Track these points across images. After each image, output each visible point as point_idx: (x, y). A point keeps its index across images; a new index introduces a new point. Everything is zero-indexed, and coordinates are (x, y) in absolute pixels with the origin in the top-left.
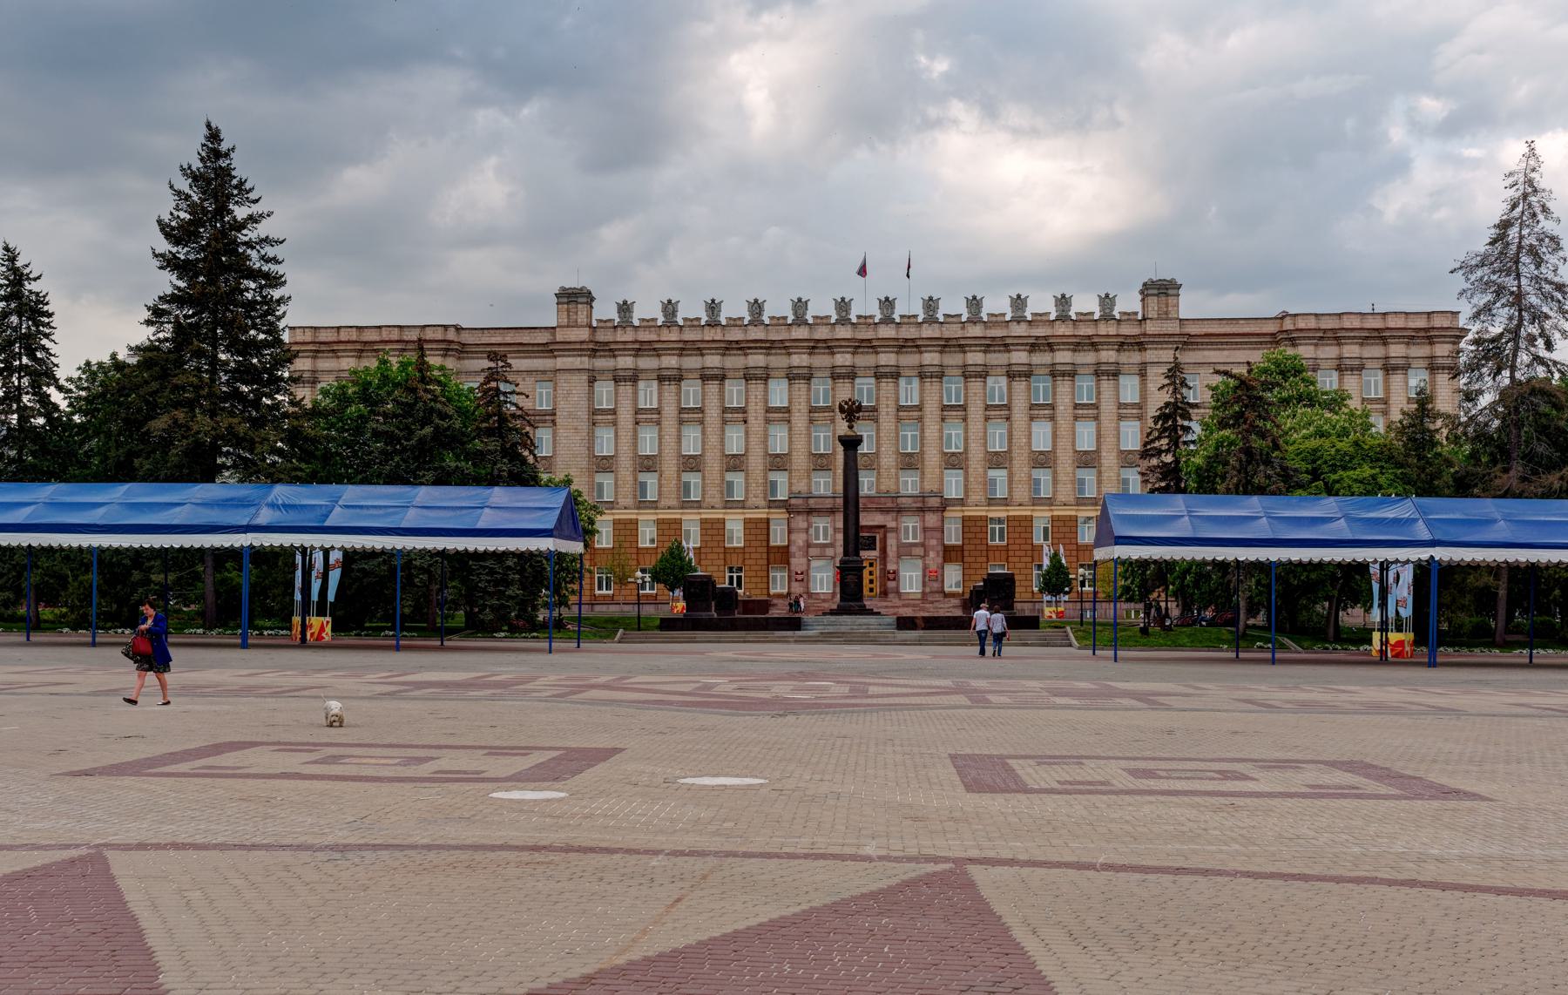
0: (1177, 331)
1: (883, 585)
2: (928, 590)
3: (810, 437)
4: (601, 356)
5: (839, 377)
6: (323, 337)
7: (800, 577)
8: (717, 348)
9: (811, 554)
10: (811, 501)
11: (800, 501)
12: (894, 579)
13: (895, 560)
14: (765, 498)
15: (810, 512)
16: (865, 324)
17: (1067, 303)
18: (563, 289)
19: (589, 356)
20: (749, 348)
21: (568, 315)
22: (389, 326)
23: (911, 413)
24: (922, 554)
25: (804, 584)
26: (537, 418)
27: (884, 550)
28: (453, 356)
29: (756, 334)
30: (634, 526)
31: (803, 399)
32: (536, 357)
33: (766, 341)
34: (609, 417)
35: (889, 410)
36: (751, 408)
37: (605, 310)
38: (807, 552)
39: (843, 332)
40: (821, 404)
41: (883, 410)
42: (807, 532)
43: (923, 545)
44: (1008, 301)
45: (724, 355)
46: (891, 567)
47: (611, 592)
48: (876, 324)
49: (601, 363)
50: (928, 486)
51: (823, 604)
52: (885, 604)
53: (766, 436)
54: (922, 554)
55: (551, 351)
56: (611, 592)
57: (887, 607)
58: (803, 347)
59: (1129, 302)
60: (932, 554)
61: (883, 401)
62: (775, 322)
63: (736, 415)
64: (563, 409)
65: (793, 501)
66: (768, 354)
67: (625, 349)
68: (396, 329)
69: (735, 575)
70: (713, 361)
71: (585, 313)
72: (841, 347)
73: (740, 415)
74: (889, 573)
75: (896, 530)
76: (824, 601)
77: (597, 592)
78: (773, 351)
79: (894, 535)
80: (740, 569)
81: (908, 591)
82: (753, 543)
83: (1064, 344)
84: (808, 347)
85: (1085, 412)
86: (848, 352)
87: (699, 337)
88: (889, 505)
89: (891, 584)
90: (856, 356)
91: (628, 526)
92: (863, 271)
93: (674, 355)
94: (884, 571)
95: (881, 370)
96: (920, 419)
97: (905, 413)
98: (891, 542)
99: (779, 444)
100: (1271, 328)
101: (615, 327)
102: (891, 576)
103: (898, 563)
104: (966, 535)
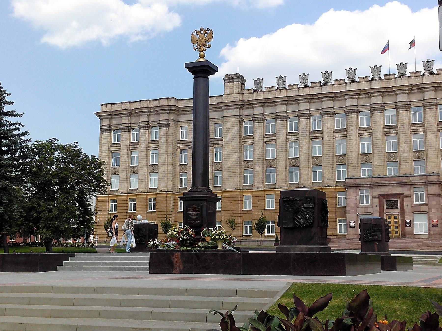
1: (403, 230)
2: (432, 233)
3: (359, 145)
4: (246, 108)
5: (374, 110)
6: (115, 108)
8: (305, 99)
10: (411, 178)
11: (352, 181)
12: (410, 226)
15: (357, 187)
16: (389, 79)
18: (227, 75)
19: (240, 108)
20: (323, 97)
21: (230, 88)
22: (144, 100)
23: (419, 128)
24: (427, 211)
26: (215, 142)
27: (403, 209)
28: (174, 113)
29: (328, 90)
30: (263, 198)
31: (354, 124)
32: (214, 111)
33: (383, 88)
34: (251, 140)
35: (405, 126)
36: (325, 130)
37: (250, 84)
38: (356, 210)
39: (377, 85)
41: (401, 127)
42: (356, 199)
43: (427, 205)
44: (276, 80)
45: (310, 102)
46: (407, 219)
47: (251, 234)
48: (395, 78)
49: (246, 112)
50: (431, 171)
53: (264, 150)
54: (427, 211)
55: (221, 107)
56: (251, 234)
58: (353, 95)
60: (433, 210)
61: (401, 122)
62: (337, 82)
63: (317, 135)
64: (226, 136)
65: (348, 181)
66: (334, 101)
67: (257, 104)
68: (129, 103)
70: (304, 106)
71: (238, 86)
72: (375, 92)
73: (320, 135)
75: (410, 196)
78: (337, 99)
79: (409, 199)
84: (356, 95)
86: (379, 96)
87: (273, 96)
89: (407, 229)
90: (385, 98)
91: (260, 198)
93: (283, 104)
94: (404, 221)
95: (426, 101)
96: (424, 131)
98: (407, 202)
99: (271, 153)
101: (346, 83)
102: (408, 224)
104: (224, 206)
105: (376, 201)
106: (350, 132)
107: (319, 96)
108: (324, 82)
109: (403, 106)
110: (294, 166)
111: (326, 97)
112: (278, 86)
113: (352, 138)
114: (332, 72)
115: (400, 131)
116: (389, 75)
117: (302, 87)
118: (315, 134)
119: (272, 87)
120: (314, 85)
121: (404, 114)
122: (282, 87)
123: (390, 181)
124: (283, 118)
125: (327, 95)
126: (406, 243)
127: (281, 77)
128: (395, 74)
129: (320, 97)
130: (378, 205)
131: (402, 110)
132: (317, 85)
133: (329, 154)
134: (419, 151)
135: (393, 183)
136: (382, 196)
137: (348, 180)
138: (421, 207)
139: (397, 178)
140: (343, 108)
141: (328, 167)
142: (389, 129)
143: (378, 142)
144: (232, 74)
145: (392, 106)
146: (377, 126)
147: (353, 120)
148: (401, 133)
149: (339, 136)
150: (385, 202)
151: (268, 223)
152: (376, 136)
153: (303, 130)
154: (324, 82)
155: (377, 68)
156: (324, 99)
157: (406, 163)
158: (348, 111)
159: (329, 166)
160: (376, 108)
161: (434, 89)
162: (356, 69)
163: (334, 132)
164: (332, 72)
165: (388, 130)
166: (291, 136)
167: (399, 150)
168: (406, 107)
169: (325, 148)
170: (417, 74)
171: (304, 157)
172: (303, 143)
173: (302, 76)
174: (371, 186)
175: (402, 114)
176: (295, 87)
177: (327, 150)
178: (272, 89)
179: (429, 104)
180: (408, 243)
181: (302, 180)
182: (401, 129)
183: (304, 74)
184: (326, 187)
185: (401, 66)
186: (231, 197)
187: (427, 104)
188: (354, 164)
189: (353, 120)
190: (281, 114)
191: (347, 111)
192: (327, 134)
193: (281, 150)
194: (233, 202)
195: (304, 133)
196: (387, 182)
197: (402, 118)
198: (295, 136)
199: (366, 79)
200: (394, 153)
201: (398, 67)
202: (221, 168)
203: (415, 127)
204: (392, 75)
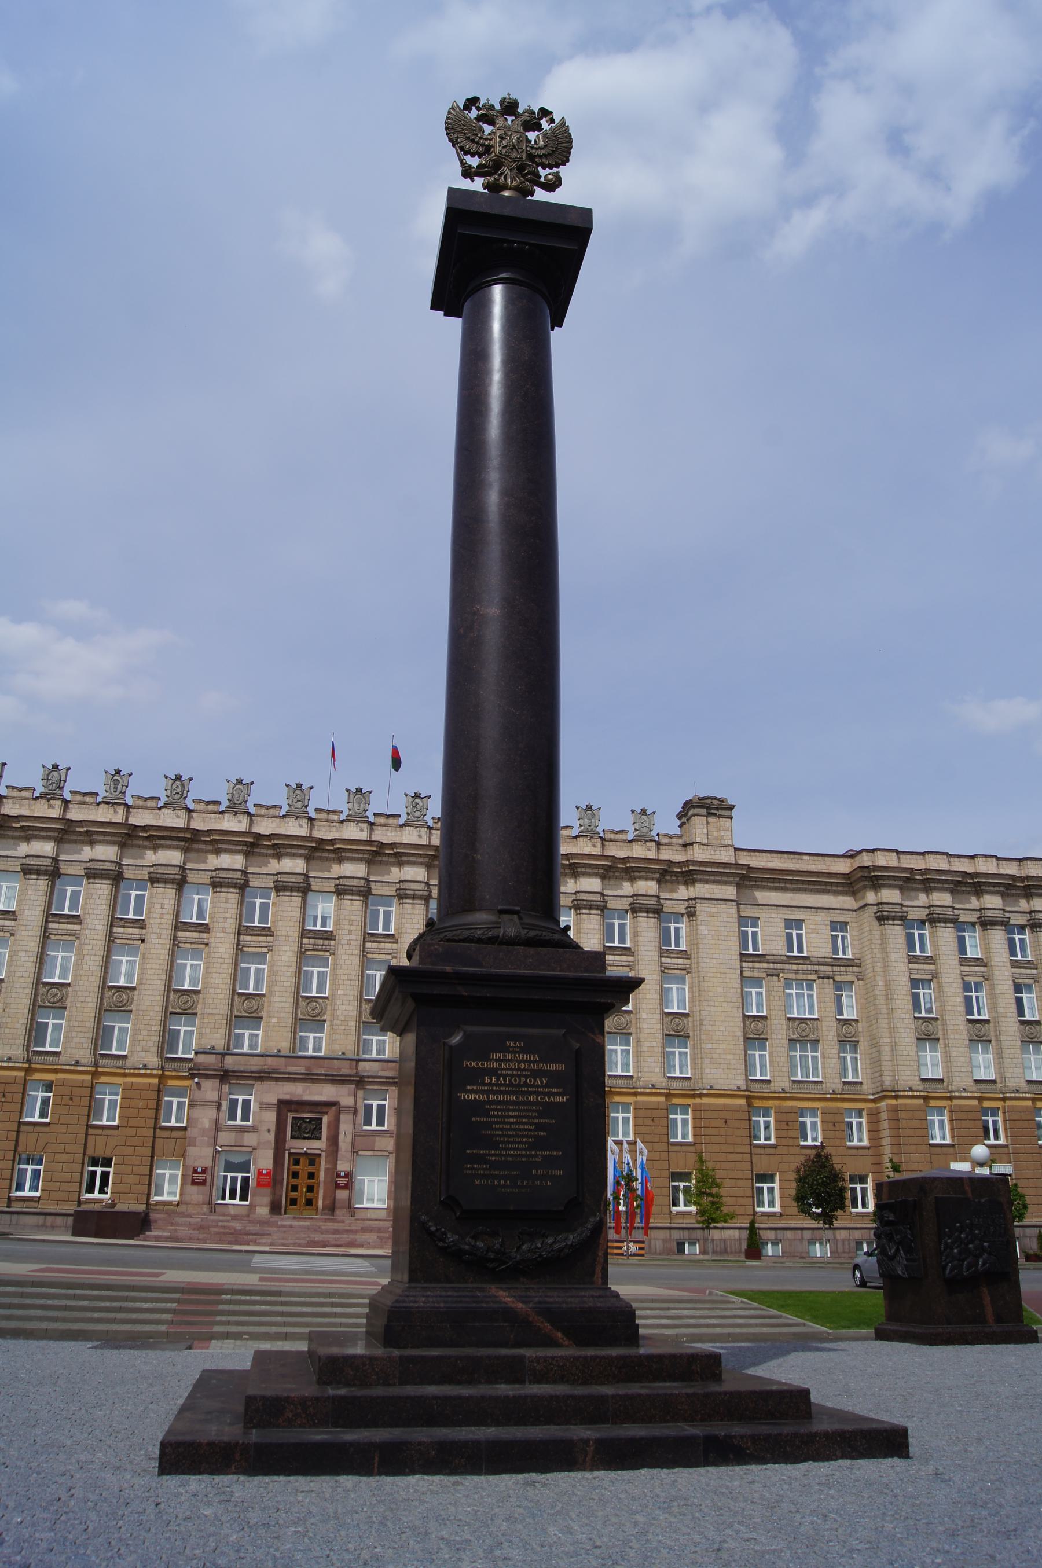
0: (597, 851)
7: (200, 1178)
9: (220, 1141)
13: (349, 1156)
14: (160, 1055)
16: (327, 821)
17: (593, 816)
23: (383, 945)
25: (205, 1189)
27: (334, 1141)
38: (216, 1138)
40: (256, 924)
44: (41, 772)
46: (343, 1167)
51: (233, 1224)
52: (331, 1226)
57: (336, 1232)
58: (238, 843)
59: (666, 824)
63: (130, 930)
65: (201, 1058)
69: (99, 1170)
72: (229, 842)
73: (137, 931)
74: (338, 1176)
76: (235, 1217)
77: (758, 1210)
80: (107, 1163)
81: (366, 1205)
82: (132, 1122)
83: (591, 866)
84: (245, 844)
85: (618, 958)
88: (346, 1071)
89: (342, 1195)
92: (396, 763)
97: (375, 945)
100: (843, 867)
102: (342, 1182)
103: (352, 1161)
104: (664, 1131)
105: (271, 1116)
106: (218, 935)
107: (338, 846)
108: (167, 799)
109: (354, 889)
110: (53, 1003)
111: (170, 838)
112: (287, 808)
113: (221, 950)
114: (191, 779)
115: (340, 947)
116: (329, 812)
117: (108, 803)
118: (124, 927)
119: (27, 789)
120: (141, 803)
121: (353, 908)
122: (54, 794)
123: (308, 1068)
124: (45, 873)
125: (174, 834)
126: (348, 1231)
127: (55, 767)
128: (34, 790)
129: (153, 836)
130: (273, 1127)
131: (350, 897)
132: (150, 804)
133: (155, 982)
134: (250, 994)
135: (317, 1074)
136: (284, 1106)
137: (203, 1055)
138: (377, 1139)
139: (326, 1061)
140: (207, 873)
141: (148, 1018)
142: (313, 938)
143: (283, 969)
144: (714, 798)
145: (328, 884)
146: (288, 929)
147: (229, 905)
148: (343, 951)
149: (189, 940)
150: (290, 1120)
151: (853, 1180)
152: (281, 953)
153: (95, 912)
154: (167, 799)
155: (302, 791)
156: (162, 842)
157: (347, 1028)
158: (221, 880)
159: (151, 1013)
160: (290, 884)
161: (1002, 889)
162: (252, 783)
163: (935, 975)
164: (191, 779)
165: (312, 941)
166: (59, 923)
167: (333, 995)
168: (360, 891)
169: (149, 966)
170: (391, 821)
171: (87, 983)
172: (90, 947)
173: (114, 776)
174: (262, 1076)
175: (348, 908)
176: (88, 799)
177: (153, 971)
178: (24, 794)
179: (412, 892)
180: (355, 1232)
181: (73, 1045)
182: (342, 942)
183: (118, 772)
184: (136, 1071)
185: (358, 796)
186: (725, 1109)
187: (408, 892)
188: (217, 1017)
189: (229, 905)
190: (41, 863)
191: (218, 880)
192: (158, 931)
193: (23, 959)
194: (721, 1123)
195: (94, 922)
196: (302, 1070)
197: (347, 917)
198: (70, 927)
199: (272, 812)
200: (321, 1001)
201: (351, 797)
202: (767, 1034)
203: (374, 942)
204: (334, 812)
